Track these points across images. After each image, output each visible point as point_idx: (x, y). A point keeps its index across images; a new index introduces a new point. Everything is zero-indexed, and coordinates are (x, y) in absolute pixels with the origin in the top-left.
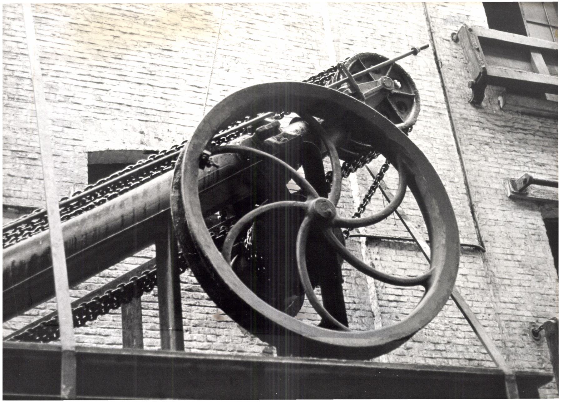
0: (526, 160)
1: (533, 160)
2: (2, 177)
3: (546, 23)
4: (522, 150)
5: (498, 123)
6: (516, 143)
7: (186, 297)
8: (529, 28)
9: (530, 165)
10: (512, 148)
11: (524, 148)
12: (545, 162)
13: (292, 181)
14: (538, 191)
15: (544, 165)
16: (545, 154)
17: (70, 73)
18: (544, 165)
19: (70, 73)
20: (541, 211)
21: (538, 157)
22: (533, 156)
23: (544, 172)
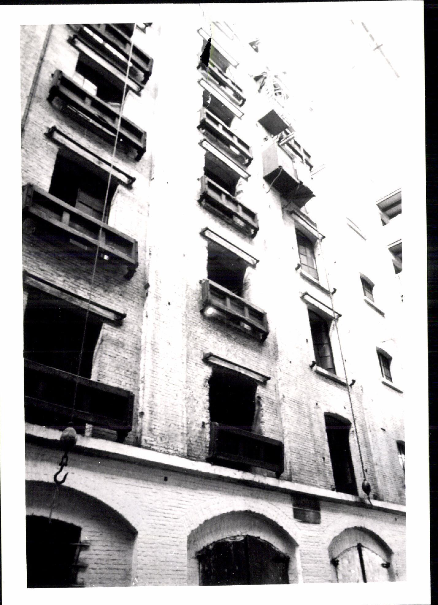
0: (34, 264)
1: (38, 266)
2: (340, 584)
3: (331, 307)
4: (35, 259)
5: (27, 240)
6: (33, 254)
7: (170, 538)
8: (78, 204)
9: (35, 268)
10: (29, 255)
11: (37, 258)
12: (45, 269)
13: (106, 326)
14: (32, 282)
15: (43, 270)
16: (48, 266)
17: (149, 185)
18: (43, 270)
19: (149, 185)
20: (29, 293)
21: (42, 266)
22: (40, 264)
23: (42, 274)
